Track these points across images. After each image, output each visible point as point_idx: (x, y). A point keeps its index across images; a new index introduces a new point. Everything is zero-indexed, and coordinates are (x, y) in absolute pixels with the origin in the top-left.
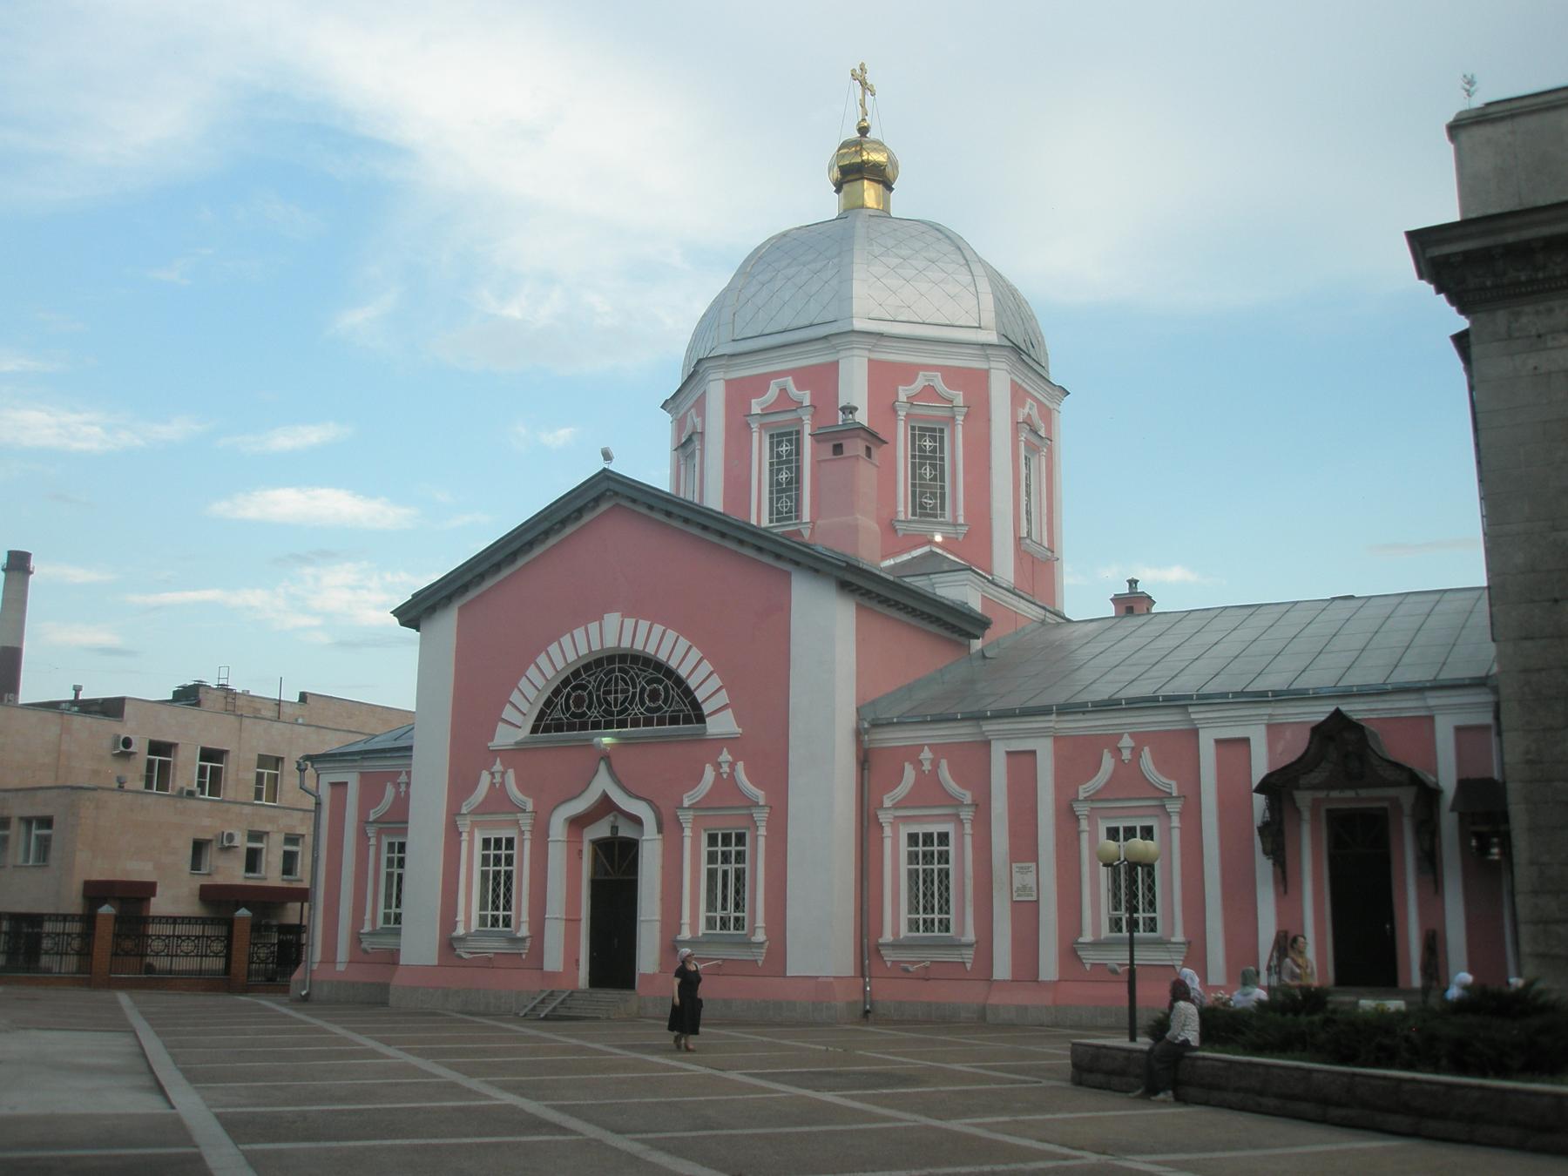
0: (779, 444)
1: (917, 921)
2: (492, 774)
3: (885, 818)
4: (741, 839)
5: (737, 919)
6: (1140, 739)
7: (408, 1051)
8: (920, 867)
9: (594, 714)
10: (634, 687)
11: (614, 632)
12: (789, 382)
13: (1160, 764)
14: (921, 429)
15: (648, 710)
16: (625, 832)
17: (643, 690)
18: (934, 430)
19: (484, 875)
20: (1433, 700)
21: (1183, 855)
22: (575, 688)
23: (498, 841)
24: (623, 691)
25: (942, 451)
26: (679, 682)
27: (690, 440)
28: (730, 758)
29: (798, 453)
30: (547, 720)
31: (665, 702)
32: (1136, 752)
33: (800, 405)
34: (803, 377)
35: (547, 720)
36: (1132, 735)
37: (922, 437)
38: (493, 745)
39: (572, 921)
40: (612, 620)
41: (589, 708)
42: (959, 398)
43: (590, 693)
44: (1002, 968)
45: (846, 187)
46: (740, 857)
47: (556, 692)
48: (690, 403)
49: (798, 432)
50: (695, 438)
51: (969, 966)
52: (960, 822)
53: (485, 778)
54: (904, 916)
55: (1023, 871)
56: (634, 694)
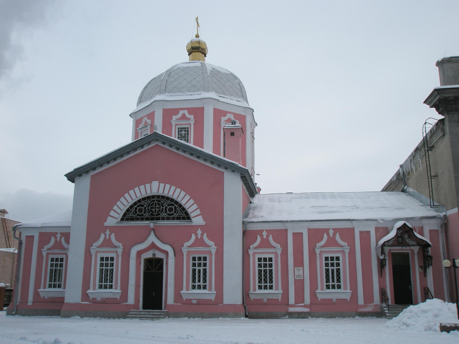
9: (164, 215)
10: (163, 206)
11: (155, 188)
12: (186, 112)
13: (342, 239)
15: (168, 214)
16: (159, 255)
17: (166, 208)
21: (349, 266)
22: (139, 206)
24: (158, 208)
26: (180, 205)
28: (201, 232)
29: (188, 135)
30: (128, 216)
31: (175, 212)
35: (128, 216)
38: (106, 224)
39: (137, 286)
40: (155, 184)
41: (145, 213)
43: (145, 208)
46: (205, 265)
51: (280, 300)
53: (103, 236)
55: (299, 270)
56: (163, 209)
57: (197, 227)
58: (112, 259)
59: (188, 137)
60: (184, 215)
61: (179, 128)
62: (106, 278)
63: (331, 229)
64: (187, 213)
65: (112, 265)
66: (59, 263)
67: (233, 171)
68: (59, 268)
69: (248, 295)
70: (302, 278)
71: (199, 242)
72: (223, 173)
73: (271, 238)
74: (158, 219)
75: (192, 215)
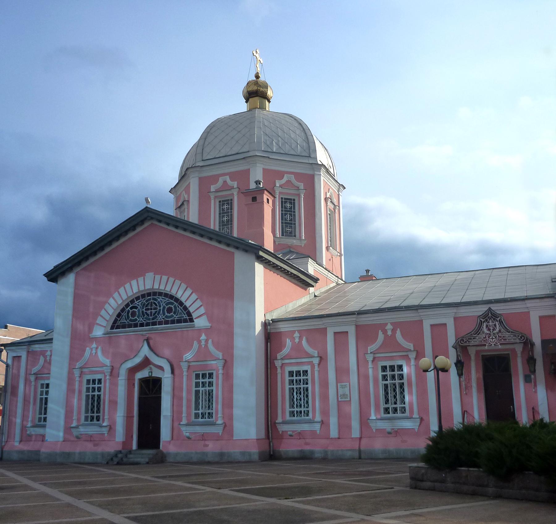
0: (223, 205)
1: (293, 412)
2: (92, 349)
3: (278, 363)
4: (211, 375)
5: (209, 413)
6: (396, 325)
7: (45, 484)
8: (295, 387)
11: (148, 282)
12: (227, 178)
14: (285, 199)
16: (156, 373)
17: (164, 308)
18: (291, 199)
19: (87, 396)
20: (529, 304)
22: (131, 308)
23: (94, 381)
25: (294, 209)
27: (183, 204)
29: (231, 209)
30: (118, 323)
32: (394, 331)
33: (233, 188)
34: (233, 176)
35: (118, 323)
36: (392, 324)
37: (286, 202)
40: (150, 276)
42: (301, 185)
44: (334, 432)
45: (250, 99)
47: (123, 310)
48: (183, 188)
49: (231, 200)
50: (185, 203)
51: (318, 432)
52: (313, 366)
54: (288, 409)
56: (160, 310)
57: (200, 331)
58: (100, 381)
59: (231, 212)
60: (186, 317)
61: (220, 202)
62: (94, 406)
63: (389, 324)
64: (189, 314)
65: (99, 389)
66: (96, 386)
67: (246, 251)
68: (96, 393)
69: (274, 424)
70: (349, 399)
71: (203, 354)
72: (234, 253)
73: (304, 342)
74: (154, 324)
75: (194, 316)
